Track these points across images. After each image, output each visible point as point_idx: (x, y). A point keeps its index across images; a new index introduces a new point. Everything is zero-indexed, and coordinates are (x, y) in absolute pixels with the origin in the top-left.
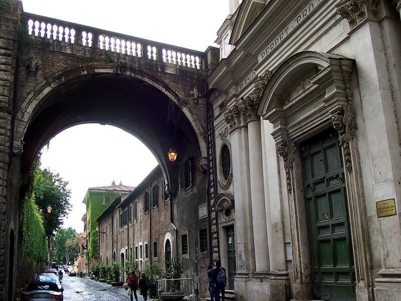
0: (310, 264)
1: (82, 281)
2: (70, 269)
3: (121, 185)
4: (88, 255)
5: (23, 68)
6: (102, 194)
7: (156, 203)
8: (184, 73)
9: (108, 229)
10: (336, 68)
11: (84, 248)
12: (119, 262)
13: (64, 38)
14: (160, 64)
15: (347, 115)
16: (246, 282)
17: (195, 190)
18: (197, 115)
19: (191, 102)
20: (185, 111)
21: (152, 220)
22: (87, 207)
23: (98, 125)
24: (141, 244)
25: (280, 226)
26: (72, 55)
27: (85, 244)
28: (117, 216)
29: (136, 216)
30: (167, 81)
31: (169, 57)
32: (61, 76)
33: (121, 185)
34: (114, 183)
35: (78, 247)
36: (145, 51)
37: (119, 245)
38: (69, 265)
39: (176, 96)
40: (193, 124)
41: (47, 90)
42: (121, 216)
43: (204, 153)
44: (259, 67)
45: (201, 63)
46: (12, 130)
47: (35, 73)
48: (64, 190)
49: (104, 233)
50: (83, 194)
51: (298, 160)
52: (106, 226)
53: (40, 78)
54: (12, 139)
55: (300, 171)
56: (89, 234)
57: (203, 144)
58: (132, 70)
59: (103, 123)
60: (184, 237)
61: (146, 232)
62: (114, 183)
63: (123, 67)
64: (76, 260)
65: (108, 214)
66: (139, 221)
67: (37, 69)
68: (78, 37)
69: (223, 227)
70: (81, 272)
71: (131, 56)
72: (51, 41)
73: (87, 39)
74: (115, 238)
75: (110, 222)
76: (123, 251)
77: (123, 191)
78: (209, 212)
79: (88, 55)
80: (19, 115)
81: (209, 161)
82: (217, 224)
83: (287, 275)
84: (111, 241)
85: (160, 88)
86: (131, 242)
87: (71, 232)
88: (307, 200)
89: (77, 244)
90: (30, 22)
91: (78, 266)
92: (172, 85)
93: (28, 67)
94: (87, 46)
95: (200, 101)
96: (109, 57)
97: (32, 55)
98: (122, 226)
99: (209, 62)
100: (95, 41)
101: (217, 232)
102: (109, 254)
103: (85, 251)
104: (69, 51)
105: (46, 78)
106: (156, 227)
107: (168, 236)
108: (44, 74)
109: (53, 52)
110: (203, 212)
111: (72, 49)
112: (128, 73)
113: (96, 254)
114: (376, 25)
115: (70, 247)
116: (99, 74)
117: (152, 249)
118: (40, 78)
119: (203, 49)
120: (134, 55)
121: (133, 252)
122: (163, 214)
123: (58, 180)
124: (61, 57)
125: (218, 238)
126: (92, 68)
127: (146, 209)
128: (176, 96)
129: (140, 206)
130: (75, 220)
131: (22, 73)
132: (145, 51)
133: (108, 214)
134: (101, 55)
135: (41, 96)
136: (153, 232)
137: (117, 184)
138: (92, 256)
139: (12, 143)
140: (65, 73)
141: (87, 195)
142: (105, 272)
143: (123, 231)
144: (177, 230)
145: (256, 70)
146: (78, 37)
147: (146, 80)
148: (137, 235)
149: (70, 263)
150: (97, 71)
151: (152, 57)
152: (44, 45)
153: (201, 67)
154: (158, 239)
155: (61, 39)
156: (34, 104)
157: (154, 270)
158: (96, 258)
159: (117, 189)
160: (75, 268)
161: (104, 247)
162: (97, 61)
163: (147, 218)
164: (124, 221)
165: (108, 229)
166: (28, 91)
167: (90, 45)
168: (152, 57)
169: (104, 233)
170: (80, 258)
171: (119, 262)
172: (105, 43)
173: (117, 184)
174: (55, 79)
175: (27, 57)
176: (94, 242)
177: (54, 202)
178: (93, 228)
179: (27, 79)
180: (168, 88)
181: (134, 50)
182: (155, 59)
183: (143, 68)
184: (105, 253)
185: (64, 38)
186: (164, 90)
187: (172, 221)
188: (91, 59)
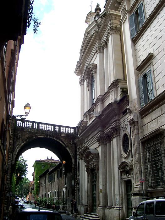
0: (92, 203)
1: (30, 206)
2: (25, 199)
3: (51, 158)
4: (34, 193)
5: (16, 137)
6: (42, 163)
7: (61, 176)
8: (68, 135)
9: (44, 183)
10: (94, 155)
11: (32, 190)
12: (47, 198)
13: (28, 126)
14: (60, 132)
15: (97, 167)
16: (81, 207)
17: (72, 174)
18: (71, 150)
19: (70, 146)
20: (68, 149)
21: (60, 182)
22: (35, 170)
23: (39, 148)
24: (55, 191)
25: (87, 192)
26: (31, 132)
27: (33, 188)
28: (47, 177)
29: (54, 179)
30: (62, 139)
31: (63, 130)
32: (27, 139)
33: (51, 158)
34: (48, 158)
35: (29, 188)
36: (54, 128)
37: (48, 190)
38: (24, 197)
39: (65, 144)
40: (70, 153)
41: (23, 144)
42: (49, 177)
43: (74, 163)
44: (85, 144)
45: (74, 131)
46: (12, 158)
47: (19, 139)
48: (25, 164)
49: (42, 184)
50: (33, 163)
51: (91, 174)
52: (43, 181)
53: (21, 140)
54: (12, 160)
55: (91, 177)
56: (35, 183)
57: (73, 160)
58: (50, 136)
59: (41, 147)
60: (68, 190)
61: (57, 186)
62: (48, 158)
63: (47, 135)
64: (28, 195)
65: (44, 175)
66: (55, 181)
67: (20, 137)
68: (33, 125)
69: (124, 181)
70: (30, 202)
71: (50, 131)
72: (24, 128)
73: (35, 126)
74: (46, 187)
75: (45, 179)
76: (49, 193)
77: (52, 162)
78: (75, 183)
79: (36, 132)
80: (14, 153)
81: (75, 166)
82: (76, 188)
83: (87, 205)
84: (44, 188)
85: (59, 141)
86: (52, 189)
87: (27, 179)
88: (92, 185)
89: (29, 187)
90: (18, 121)
91: (29, 198)
92: (63, 140)
93: (17, 137)
94: (35, 128)
95: (73, 145)
96: (43, 131)
97: (19, 133)
98: (49, 182)
99: (77, 131)
100: (38, 126)
101: (76, 190)
102: (44, 194)
103: (33, 191)
104: (30, 131)
105: (22, 140)
106: (61, 185)
107: (64, 189)
108: (22, 139)
109: (25, 131)
110: (73, 183)
111: (31, 130)
112: (49, 137)
113: (37, 193)
114: (103, 146)
115: (25, 188)
116: (39, 137)
117: (59, 193)
118: (21, 140)
119: (75, 127)
120: (51, 130)
121: (52, 193)
122: (63, 180)
123: (22, 160)
124: (27, 133)
125: (76, 192)
126: (37, 136)
127: (58, 177)
128: (65, 144)
129: (56, 175)
130: (29, 176)
131: (15, 139)
132: (54, 128)
133: (44, 175)
134: (40, 131)
135: (21, 146)
136: (60, 186)
137: (50, 158)
138: (36, 194)
139: (12, 162)
140: (28, 138)
141: (35, 163)
142: (41, 202)
143: (49, 184)
144: (66, 188)
145: (84, 144)
146: (33, 125)
147: (55, 139)
148: (54, 187)
149: (25, 196)
150: (38, 137)
151: (57, 130)
152: (22, 129)
153: (74, 133)
154: (61, 190)
155: (27, 127)
156: (19, 148)
157: (58, 203)
158: (38, 195)
159: (49, 161)
160: (27, 199)
161: (42, 190)
162: (38, 133)
163: (58, 180)
164: (50, 180)
165: (44, 183)
166: (17, 145)
167: (36, 128)
168: (57, 130)
169: (42, 184)
170: (30, 194)
171: (47, 198)
172: (41, 127)
173: (50, 158)
174: (25, 140)
175: (16, 134)
176: (37, 187)
177: (22, 170)
178: (37, 180)
179: (17, 141)
180: (62, 141)
181: (51, 128)
182: (58, 131)
183: (54, 135)
184: (42, 193)
185: (28, 126)
186: (60, 142)
187: (65, 184)
188: (37, 133)
